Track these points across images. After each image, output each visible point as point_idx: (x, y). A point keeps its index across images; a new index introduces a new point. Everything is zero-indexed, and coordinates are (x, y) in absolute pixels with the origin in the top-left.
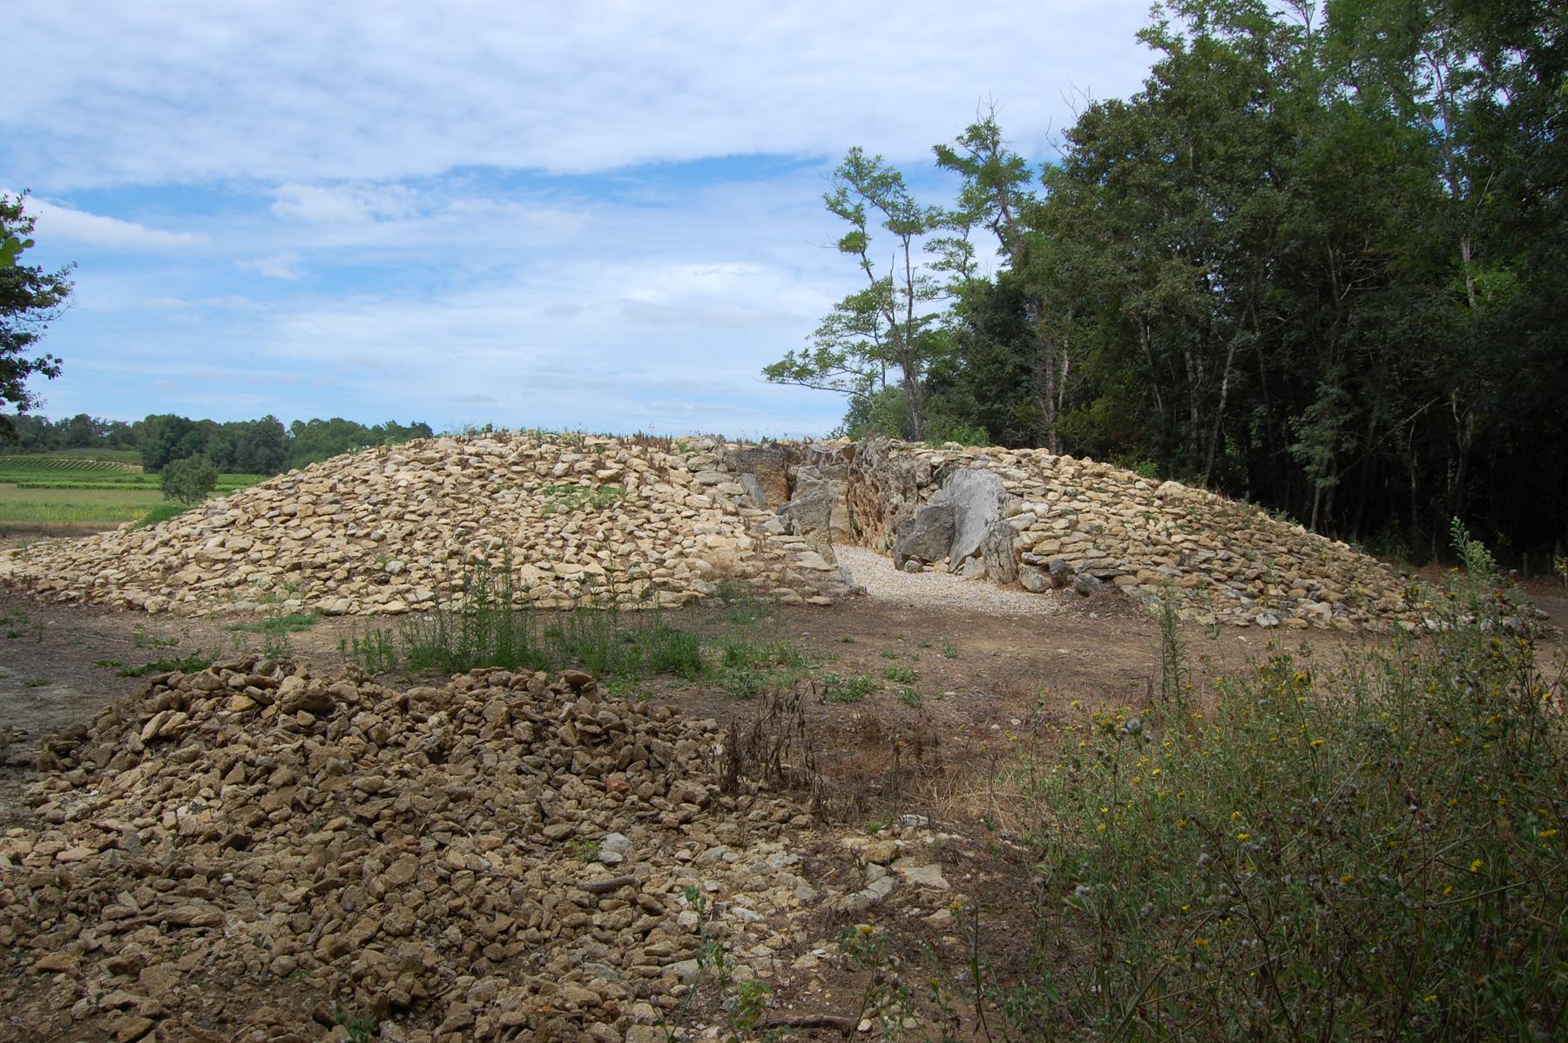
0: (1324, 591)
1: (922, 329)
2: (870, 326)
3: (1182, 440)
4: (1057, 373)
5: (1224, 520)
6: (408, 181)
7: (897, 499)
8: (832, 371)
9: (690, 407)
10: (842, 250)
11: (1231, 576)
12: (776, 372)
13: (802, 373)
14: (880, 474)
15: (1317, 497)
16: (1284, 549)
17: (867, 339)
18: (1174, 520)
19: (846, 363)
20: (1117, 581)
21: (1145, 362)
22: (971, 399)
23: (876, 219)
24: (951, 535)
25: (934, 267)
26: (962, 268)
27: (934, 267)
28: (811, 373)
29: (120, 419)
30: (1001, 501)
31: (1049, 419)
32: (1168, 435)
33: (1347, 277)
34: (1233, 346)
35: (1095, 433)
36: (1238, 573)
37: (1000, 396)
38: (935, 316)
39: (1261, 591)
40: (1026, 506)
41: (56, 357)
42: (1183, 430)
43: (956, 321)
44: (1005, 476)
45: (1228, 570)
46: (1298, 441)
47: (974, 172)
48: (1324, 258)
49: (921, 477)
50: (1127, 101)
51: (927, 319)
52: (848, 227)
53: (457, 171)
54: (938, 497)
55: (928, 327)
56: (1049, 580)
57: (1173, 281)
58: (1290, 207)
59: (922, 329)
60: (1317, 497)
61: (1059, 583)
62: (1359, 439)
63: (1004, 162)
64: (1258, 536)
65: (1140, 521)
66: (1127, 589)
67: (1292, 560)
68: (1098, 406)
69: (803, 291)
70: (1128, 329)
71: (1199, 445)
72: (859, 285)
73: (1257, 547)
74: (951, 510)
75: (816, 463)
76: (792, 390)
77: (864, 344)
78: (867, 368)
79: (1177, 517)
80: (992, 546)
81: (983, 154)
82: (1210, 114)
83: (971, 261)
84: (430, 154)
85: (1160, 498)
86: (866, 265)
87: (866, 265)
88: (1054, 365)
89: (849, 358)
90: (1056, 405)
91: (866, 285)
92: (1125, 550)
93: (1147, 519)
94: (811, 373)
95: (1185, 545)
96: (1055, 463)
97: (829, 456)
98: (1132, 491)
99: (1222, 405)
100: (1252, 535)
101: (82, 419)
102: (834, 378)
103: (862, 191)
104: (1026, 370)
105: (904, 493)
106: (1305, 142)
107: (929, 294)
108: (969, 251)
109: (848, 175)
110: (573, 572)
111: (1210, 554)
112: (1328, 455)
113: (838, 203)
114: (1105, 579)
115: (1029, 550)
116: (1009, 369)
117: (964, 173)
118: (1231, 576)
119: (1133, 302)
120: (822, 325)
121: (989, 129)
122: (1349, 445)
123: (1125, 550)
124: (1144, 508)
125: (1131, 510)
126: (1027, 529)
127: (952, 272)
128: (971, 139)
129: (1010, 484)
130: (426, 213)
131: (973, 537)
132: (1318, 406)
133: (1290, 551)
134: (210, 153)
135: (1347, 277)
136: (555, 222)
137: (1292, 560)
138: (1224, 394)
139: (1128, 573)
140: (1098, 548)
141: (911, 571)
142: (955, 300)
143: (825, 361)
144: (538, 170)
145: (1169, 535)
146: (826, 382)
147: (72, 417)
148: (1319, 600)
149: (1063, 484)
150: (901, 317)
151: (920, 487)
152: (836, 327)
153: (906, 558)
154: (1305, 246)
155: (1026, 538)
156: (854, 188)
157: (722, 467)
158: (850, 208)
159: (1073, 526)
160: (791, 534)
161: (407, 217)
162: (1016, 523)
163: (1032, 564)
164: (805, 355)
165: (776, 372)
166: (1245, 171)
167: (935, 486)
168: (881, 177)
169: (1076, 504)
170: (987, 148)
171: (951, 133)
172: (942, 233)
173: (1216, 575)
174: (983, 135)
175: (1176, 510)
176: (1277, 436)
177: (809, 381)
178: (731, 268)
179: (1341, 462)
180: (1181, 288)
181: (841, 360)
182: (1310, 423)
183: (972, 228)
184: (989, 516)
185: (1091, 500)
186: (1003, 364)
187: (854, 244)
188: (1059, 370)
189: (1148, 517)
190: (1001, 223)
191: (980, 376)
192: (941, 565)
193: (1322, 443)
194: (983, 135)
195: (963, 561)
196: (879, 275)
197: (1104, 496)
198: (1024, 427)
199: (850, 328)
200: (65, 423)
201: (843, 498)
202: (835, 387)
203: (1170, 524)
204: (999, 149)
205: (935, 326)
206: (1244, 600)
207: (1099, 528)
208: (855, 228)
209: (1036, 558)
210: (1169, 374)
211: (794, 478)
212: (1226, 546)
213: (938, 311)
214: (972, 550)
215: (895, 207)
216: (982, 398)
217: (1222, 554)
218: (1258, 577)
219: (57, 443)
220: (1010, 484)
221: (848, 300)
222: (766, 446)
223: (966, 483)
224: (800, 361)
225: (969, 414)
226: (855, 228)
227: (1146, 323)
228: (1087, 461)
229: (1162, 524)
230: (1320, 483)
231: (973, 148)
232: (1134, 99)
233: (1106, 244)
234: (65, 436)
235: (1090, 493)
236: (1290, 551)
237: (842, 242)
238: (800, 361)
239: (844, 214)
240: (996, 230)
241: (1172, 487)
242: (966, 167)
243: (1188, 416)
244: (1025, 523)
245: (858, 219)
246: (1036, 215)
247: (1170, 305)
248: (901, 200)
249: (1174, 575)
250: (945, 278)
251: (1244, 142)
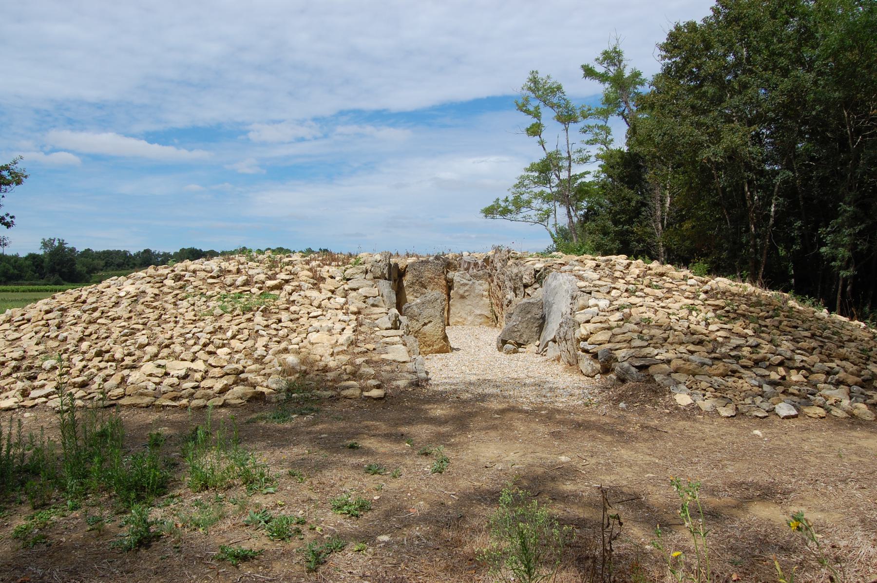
0: (842, 375)
1: (579, 181)
2: (547, 181)
3: (742, 246)
4: (663, 205)
5: (757, 310)
6: (316, 119)
7: (510, 295)
8: (523, 210)
9: (473, 236)
10: (529, 135)
11: (757, 363)
12: (489, 212)
13: (505, 212)
14: (501, 276)
15: (841, 283)
16: (807, 334)
17: (544, 189)
18: (715, 311)
19: (533, 205)
20: (651, 370)
21: (717, 194)
22: (609, 223)
23: (548, 115)
24: (542, 323)
25: (587, 143)
26: (605, 143)
27: (587, 143)
28: (510, 212)
29: (167, 251)
30: (573, 298)
31: (658, 237)
32: (735, 243)
33: (858, 132)
34: (778, 180)
35: (687, 243)
36: (764, 359)
37: (630, 222)
38: (589, 173)
39: (783, 378)
40: (592, 302)
41: (11, 215)
42: (744, 240)
43: (603, 176)
44: (581, 278)
45: (754, 357)
46: (825, 245)
47: (607, 80)
48: (841, 119)
49: (527, 279)
50: (699, 22)
51: (582, 175)
52: (530, 120)
53: (342, 113)
54: (537, 294)
55: (583, 180)
56: (598, 366)
57: (734, 136)
58: (815, 83)
59: (579, 181)
60: (841, 283)
61: (606, 370)
62: (869, 242)
63: (627, 73)
64: (785, 323)
65: (684, 313)
66: (658, 378)
67: (814, 344)
68: (687, 225)
69: (501, 163)
70: (706, 173)
71: (756, 250)
72: (539, 156)
73: (784, 333)
74: (542, 305)
75: (467, 269)
76: (499, 221)
77: (542, 193)
78: (545, 207)
79: (717, 308)
80: (562, 335)
81: (612, 68)
82: (757, 25)
83: (610, 137)
84: (327, 105)
85: (706, 292)
86: (542, 143)
87: (542, 143)
88: (661, 201)
89: (534, 200)
90: (663, 226)
91: (543, 155)
92: (665, 340)
93: (690, 312)
94: (510, 212)
95: (719, 333)
96: (629, 265)
97: (476, 264)
98: (684, 287)
99: (771, 221)
100: (780, 322)
101: (147, 251)
102: (524, 214)
103: (537, 97)
104: (644, 205)
105: (515, 291)
106: (824, 36)
107: (585, 160)
108: (608, 132)
109: (530, 88)
110: (178, 368)
111: (741, 341)
112: (847, 254)
113: (524, 106)
114: (641, 368)
115: (585, 340)
116: (633, 204)
117: (601, 81)
118: (757, 363)
119: (705, 154)
120: (517, 182)
121: (616, 52)
122: (862, 246)
123: (665, 340)
124: (690, 302)
125: (678, 304)
126: (588, 322)
127: (599, 146)
128: (605, 59)
129: (582, 284)
130: (326, 136)
131: (552, 329)
132: (839, 220)
133: (813, 336)
134: (213, 110)
135: (858, 132)
136: (395, 136)
137: (814, 344)
138: (772, 214)
139: (663, 362)
140: (642, 338)
141: (508, 353)
142: (600, 162)
143: (519, 204)
144: (384, 110)
145: (708, 324)
146: (519, 217)
147: (142, 251)
148: (838, 384)
149: (628, 283)
150: (564, 175)
151: (526, 286)
152: (526, 182)
153: (504, 342)
154: (826, 111)
155: (583, 331)
156: (533, 95)
157: (370, 276)
158: (532, 109)
159: (625, 319)
160: (397, 328)
161: (316, 138)
162: (580, 317)
163: (586, 351)
164: (506, 200)
165: (489, 212)
166: (783, 62)
167: (537, 286)
168: (550, 88)
169: (633, 300)
170: (615, 65)
171: (591, 56)
172: (591, 122)
173: (744, 362)
174: (612, 57)
175: (717, 302)
176: (811, 241)
177: (509, 216)
178: (493, 158)
179: (856, 258)
180: (738, 141)
181: (528, 203)
182: (833, 232)
183: (610, 118)
184: (564, 310)
185: (647, 295)
186: (630, 201)
187: (535, 131)
188: (664, 202)
189: (691, 309)
190: (626, 112)
191: (617, 208)
192: (532, 347)
193: (843, 246)
194: (612, 57)
195: (546, 346)
196: (551, 148)
197: (658, 293)
198: (644, 241)
199: (535, 183)
200: (138, 254)
201: (486, 293)
202: (525, 219)
203: (710, 314)
204: (622, 64)
205: (588, 179)
206: (767, 388)
207: (648, 320)
208: (535, 121)
209: (589, 347)
210: (733, 203)
211: (452, 281)
212: (757, 333)
213: (591, 171)
214: (552, 337)
215: (559, 106)
216: (616, 223)
217: (752, 341)
218: (781, 364)
219: (135, 265)
220: (582, 284)
221: (532, 165)
222: (431, 258)
223: (554, 284)
224: (503, 204)
225: (609, 233)
226: (535, 121)
227: (718, 169)
228: (655, 265)
229: (702, 315)
230: (843, 274)
231: (605, 65)
232: (705, 20)
233: (687, 117)
234: (138, 261)
235: (647, 290)
236: (813, 336)
237: (528, 130)
238: (503, 204)
239: (528, 112)
240: (624, 118)
241: (722, 282)
242: (603, 78)
243: (748, 229)
244: (588, 317)
245: (537, 115)
246: (644, 104)
247: (732, 155)
248: (562, 101)
249: (703, 364)
250: (594, 150)
251: (780, 41)
